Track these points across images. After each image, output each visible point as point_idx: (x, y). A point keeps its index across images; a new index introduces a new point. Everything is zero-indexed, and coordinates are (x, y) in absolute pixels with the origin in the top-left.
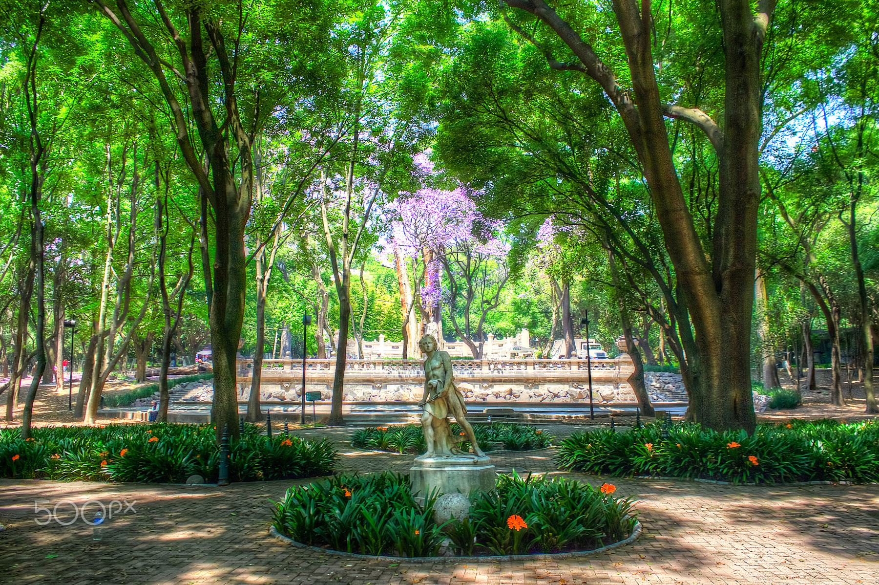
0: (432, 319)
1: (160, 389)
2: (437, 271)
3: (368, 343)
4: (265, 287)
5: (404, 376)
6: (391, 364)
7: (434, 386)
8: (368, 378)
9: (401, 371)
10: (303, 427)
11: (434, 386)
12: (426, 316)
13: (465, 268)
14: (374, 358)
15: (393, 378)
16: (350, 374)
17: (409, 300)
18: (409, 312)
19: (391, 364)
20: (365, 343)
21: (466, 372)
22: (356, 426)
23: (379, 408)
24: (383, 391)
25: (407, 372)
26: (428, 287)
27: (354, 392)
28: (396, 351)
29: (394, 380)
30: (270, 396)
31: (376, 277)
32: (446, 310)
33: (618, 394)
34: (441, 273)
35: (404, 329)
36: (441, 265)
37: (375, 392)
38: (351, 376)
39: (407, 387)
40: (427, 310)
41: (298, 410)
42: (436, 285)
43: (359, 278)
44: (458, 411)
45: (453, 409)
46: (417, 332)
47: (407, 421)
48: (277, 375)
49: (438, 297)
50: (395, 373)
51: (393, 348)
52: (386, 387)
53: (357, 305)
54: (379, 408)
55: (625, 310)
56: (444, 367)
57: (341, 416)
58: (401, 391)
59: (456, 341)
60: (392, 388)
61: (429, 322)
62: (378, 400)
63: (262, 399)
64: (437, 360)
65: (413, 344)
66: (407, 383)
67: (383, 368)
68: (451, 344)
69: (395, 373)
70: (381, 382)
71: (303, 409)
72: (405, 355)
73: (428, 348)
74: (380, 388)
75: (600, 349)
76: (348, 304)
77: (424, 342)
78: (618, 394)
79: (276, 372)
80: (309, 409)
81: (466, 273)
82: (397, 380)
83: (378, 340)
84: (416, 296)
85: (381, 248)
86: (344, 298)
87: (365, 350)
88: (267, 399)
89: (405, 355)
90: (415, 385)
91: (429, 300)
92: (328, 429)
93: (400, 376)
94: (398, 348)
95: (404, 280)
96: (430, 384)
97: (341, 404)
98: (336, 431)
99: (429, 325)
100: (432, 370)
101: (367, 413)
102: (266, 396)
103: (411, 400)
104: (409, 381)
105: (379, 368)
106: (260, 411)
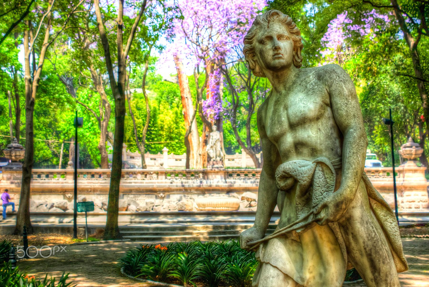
0: (214, 127)
1: (257, 200)
2: (218, 84)
3: (153, 156)
4: (34, 89)
5: (186, 185)
6: (176, 174)
7: (304, 181)
8: (151, 188)
9: (184, 181)
10: (75, 241)
11: (304, 181)
12: (209, 125)
13: (246, 79)
14: (157, 169)
15: (176, 188)
16: (133, 184)
17: (191, 110)
18: (192, 122)
19: (176, 174)
20: (148, 156)
21: (249, 181)
22: (133, 240)
23: (162, 218)
24: (166, 200)
25: (190, 181)
26: (210, 100)
27: (138, 202)
28: (179, 163)
29: (177, 190)
30: (52, 206)
31: (160, 94)
32: (227, 124)
33: (402, 202)
34: (222, 87)
35: (186, 139)
36: (222, 76)
37: (157, 202)
38: (134, 186)
39: (190, 196)
40: (209, 120)
41: (68, 221)
42: (217, 98)
43: (143, 96)
44: (384, 268)
45: (365, 261)
46: (199, 144)
47: (191, 234)
48: (59, 186)
49: (219, 109)
50: (178, 182)
51: (176, 160)
52: (168, 197)
53: (141, 120)
54: (162, 218)
55: (103, 231)
56: (334, 117)
57: (118, 229)
58: (184, 200)
59: (235, 153)
60: (174, 197)
61: (211, 131)
62: (161, 210)
63: (33, 209)
64: (309, 92)
65: (195, 156)
66: (191, 193)
67: (166, 178)
68: (230, 157)
69: (178, 182)
70: (164, 191)
71: (75, 220)
72: (188, 166)
73: (276, 56)
74: (163, 198)
75: (375, 159)
76: (123, 104)
77: (260, 34)
78: (402, 202)
79: (58, 183)
80: (81, 221)
81: (247, 85)
82: (180, 190)
83: (162, 152)
84: (200, 108)
85: (161, 48)
86: (119, 96)
87: (148, 161)
88: (50, 208)
89: (188, 166)
90: (199, 194)
91: (210, 113)
92: (102, 244)
93: (183, 186)
94: (180, 160)
95: (186, 94)
96: (286, 176)
97: (117, 214)
98: (110, 246)
99: (211, 134)
100: (293, 126)
101: (147, 225)
102: (49, 206)
103: (195, 210)
104: (193, 191)
105: (162, 178)
106: (30, 222)
